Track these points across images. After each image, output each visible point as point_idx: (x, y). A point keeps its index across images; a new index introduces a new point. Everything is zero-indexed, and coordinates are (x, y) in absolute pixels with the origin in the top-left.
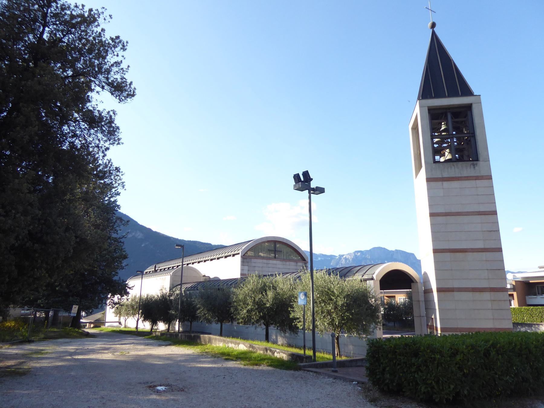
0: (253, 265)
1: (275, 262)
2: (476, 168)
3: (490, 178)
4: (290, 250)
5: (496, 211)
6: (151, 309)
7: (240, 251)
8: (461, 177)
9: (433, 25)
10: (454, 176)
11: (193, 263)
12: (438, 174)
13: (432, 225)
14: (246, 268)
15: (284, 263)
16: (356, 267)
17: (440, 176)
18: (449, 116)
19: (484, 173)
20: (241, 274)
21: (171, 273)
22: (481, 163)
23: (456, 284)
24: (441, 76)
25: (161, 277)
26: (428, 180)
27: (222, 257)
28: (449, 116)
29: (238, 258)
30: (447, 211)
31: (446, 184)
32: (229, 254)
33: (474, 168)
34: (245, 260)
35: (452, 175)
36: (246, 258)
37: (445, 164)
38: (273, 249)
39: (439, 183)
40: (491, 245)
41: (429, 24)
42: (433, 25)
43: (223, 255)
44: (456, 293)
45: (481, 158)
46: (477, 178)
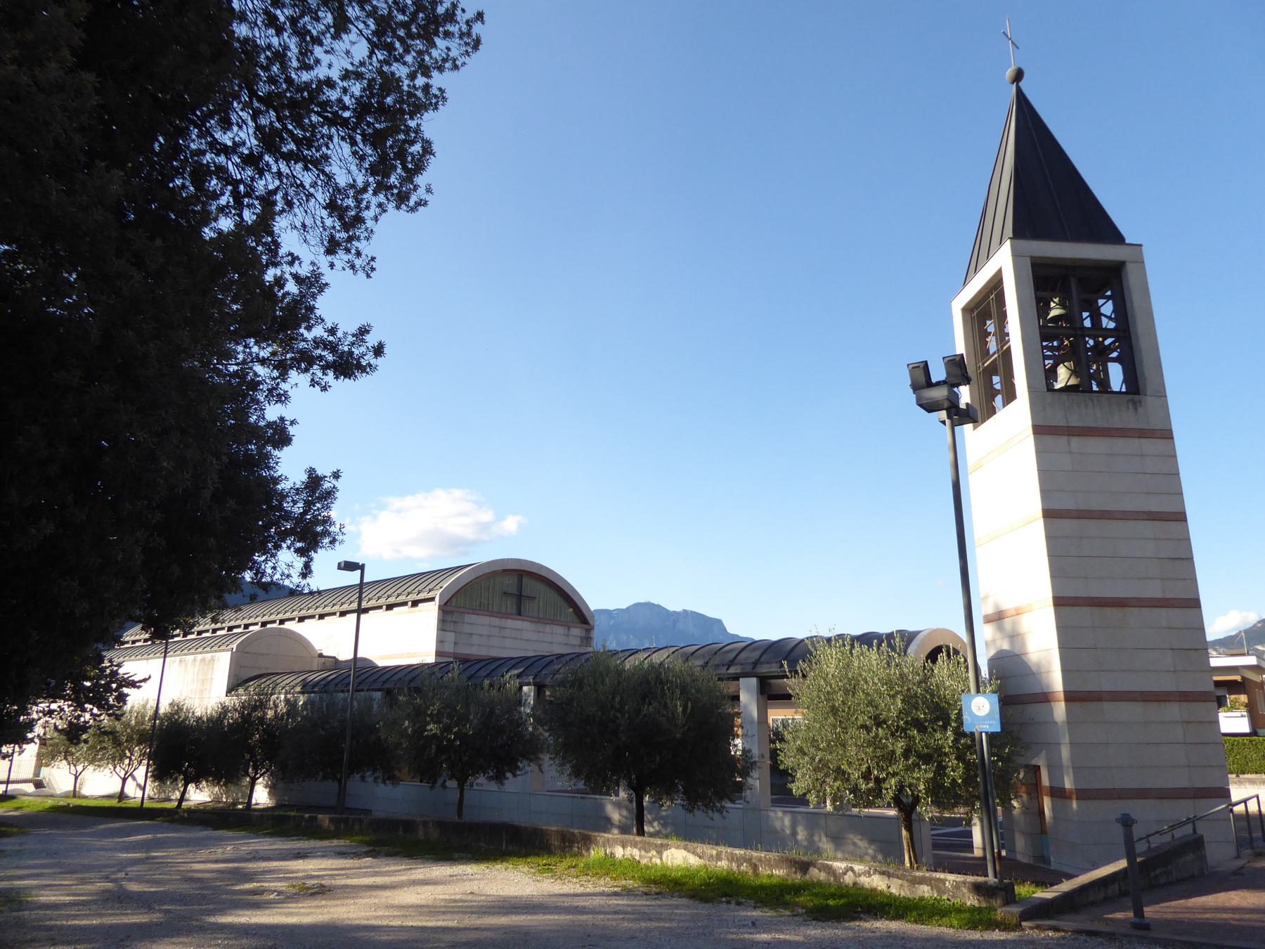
0: (467, 629)
1: (518, 624)
2: (1140, 410)
3: (1168, 435)
4: (553, 595)
5: (1185, 513)
6: (178, 746)
7: (437, 594)
8: (1108, 429)
9: (1019, 76)
10: (1093, 425)
11: (301, 619)
12: (1058, 419)
13: (1049, 538)
14: (451, 636)
15: (540, 627)
16: (637, 651)
17: (1062, 423)
18: (1073, 284)
19: (1156, 424)
20: (438, 654)
21: (235, 647)
22: (1150, 401)
23: (1106, 684)
24: (1049, 193)
25: (199, 657)
26: (1038, 430)
27: (334, 614)
28: (1073, 284)
29: (430, 612)
30: (1082, 507)
31: (1076, 442)
32: (311, 612)
33: (1136, 409)
34: (449, 618)
35: (1089, 422)
36: (452, 612)
37: (1064, 396)
38: (515, 591)
39: (1063, 439)
40: (1176, 591)
41: (1010, 73)
42: (1019, 76)
43: (336, 608)
44: (1107, 706)
45: (1150, 389)
46: (1144, 434)
